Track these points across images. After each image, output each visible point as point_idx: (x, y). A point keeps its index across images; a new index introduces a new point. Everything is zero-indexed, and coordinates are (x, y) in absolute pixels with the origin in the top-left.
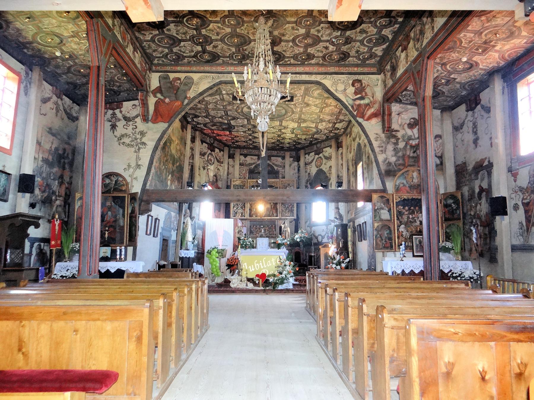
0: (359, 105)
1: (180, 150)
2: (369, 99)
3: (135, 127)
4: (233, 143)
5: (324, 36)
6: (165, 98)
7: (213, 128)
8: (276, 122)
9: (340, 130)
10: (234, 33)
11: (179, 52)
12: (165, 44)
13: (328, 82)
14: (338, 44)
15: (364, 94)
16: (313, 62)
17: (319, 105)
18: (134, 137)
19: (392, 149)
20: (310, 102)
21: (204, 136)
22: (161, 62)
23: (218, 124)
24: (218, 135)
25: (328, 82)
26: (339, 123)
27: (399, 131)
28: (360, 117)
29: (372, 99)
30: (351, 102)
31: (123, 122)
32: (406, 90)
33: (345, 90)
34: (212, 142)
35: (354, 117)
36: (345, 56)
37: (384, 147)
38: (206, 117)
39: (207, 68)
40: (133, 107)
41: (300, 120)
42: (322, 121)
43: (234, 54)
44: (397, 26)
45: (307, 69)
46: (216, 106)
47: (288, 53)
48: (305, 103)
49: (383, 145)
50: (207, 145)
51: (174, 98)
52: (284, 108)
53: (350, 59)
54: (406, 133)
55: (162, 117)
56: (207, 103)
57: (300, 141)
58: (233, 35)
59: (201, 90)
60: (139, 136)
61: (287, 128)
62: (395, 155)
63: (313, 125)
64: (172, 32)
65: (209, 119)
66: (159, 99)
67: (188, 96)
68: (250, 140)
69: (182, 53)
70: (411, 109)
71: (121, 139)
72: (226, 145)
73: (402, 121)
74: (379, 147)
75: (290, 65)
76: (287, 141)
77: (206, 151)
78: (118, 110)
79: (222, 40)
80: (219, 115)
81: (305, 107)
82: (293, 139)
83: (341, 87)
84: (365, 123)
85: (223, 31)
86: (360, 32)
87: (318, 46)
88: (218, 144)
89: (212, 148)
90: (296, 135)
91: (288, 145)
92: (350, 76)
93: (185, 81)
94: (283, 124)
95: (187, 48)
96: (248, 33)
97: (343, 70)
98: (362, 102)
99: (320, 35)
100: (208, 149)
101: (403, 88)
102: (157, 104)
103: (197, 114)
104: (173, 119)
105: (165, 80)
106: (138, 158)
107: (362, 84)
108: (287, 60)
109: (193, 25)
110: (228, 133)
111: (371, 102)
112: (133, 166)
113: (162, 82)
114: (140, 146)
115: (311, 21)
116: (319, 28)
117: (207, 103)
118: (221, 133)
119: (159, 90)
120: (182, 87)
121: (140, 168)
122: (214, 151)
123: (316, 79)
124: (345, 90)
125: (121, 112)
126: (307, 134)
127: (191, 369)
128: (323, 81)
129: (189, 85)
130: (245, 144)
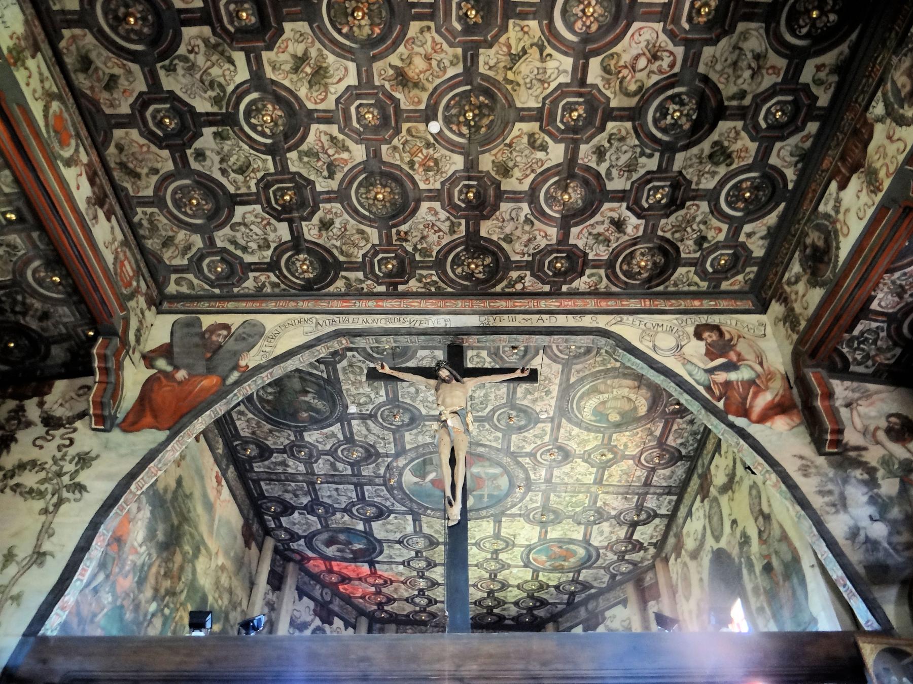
0: (727, 384)
1: (230, 591)
2: (752, 368)
3: (67, 442)
4: (380, 605)
5: (615, 172)
6: (177, 368)
7: (331, 551)
8: (484, 523)
9: (646, 550)
10: (374, 166)
11: (231, 248)
12: (193, 216)
13: (629, 329)
14: (651, 207)
15: (733, 356)
16: (582, 283)
17: (596, 457)
18: (55, 468)
19: (865, 499)
20: (573, 445)
21: (307, 579)
22: (184, 289)
23: (342, 537)
24: (345, 579)
25: (629, 329)
26: (645, 523)
27: (865, 449)
28: (738, 415)
29: (758, 368)
30: (702, 377)
31: (40, 430)
32: (864, 312)
33: (679, 347)
34: (328, 598)
35: (721, 416)
36: (668, 256)
37: (836, 492)
38: (310, 509)
39: (304, 305)
40: (81, 392)
41: (547, 516)
42: (601, 516)
43: (376, 253)
44: (812, 127)
45: (569, 304)
46: (333, 466)
47: (518, 247)
48: (560, 448)
49: (830, 486)
50: (312, 604)
51: (201, 368)
52: (507, 472)
53: (681, 270)
54: (891, 455)
55: (155, 417)
56: (311, 456)
57: (543, 595)
58: (375, 172)
59: (281, 348)
60: (69, 467)
61: (514, 545)
62: (882, 518)
63: (578, 535)
64: (208, 163)
65: (319, 517)
66: (161, 371)
67: (242, 363)
68: (421, 592)
69: (239, 253)
70: (876, 393)
71: (12, 477)
72: (361, 612)
73: (867, 422)
74: (822, 493)
75: (523, 294)
76: (513, 595)
77: (309, 618)
78: (35, 400)
79: (340, 196)
80: (343, 502)
81: (560, 464)
82: (527, 587)
83: (666, 341)
84: (755, 430)
85: (345, 155)
86: (711, 156)
87: (598, 218)
88: (341, 607)
89: (325, 614)
90: (536, 572)
91: (513, 611)
92: (685, 317)
93: (241, 331)
94: (504, 532)
95: (254, 231)
96: (412, 164)
97: (661, 304)
98: (733, 376)
99: (602, 169)
100: (316, 613)
101: (856, 306)
102: (148, 384)
103: (288, 497)
104: (185, 420)
105: (186, 330)
106: (46, 531)
107: (721, 334)
108: (514, 274)
109: (263, 134)
110: (365, 568)
111: (758, 376)
112: (19, 559)
113: (176, 335)
114: (65, 494)
115: (581, 112)
116: (601, 139)
117: (311, 456)
118: (349, 569)
119: (166, 351)
120: (231, 345)
121: (41, 564)
122: (331, 623)
123: (594, 325)
124: (679, 347)
125: (41, 404)
126: (561, 569)
127: (753, 473)
128: (615, 329)
129: (251, 340)
130: (408, 608)
